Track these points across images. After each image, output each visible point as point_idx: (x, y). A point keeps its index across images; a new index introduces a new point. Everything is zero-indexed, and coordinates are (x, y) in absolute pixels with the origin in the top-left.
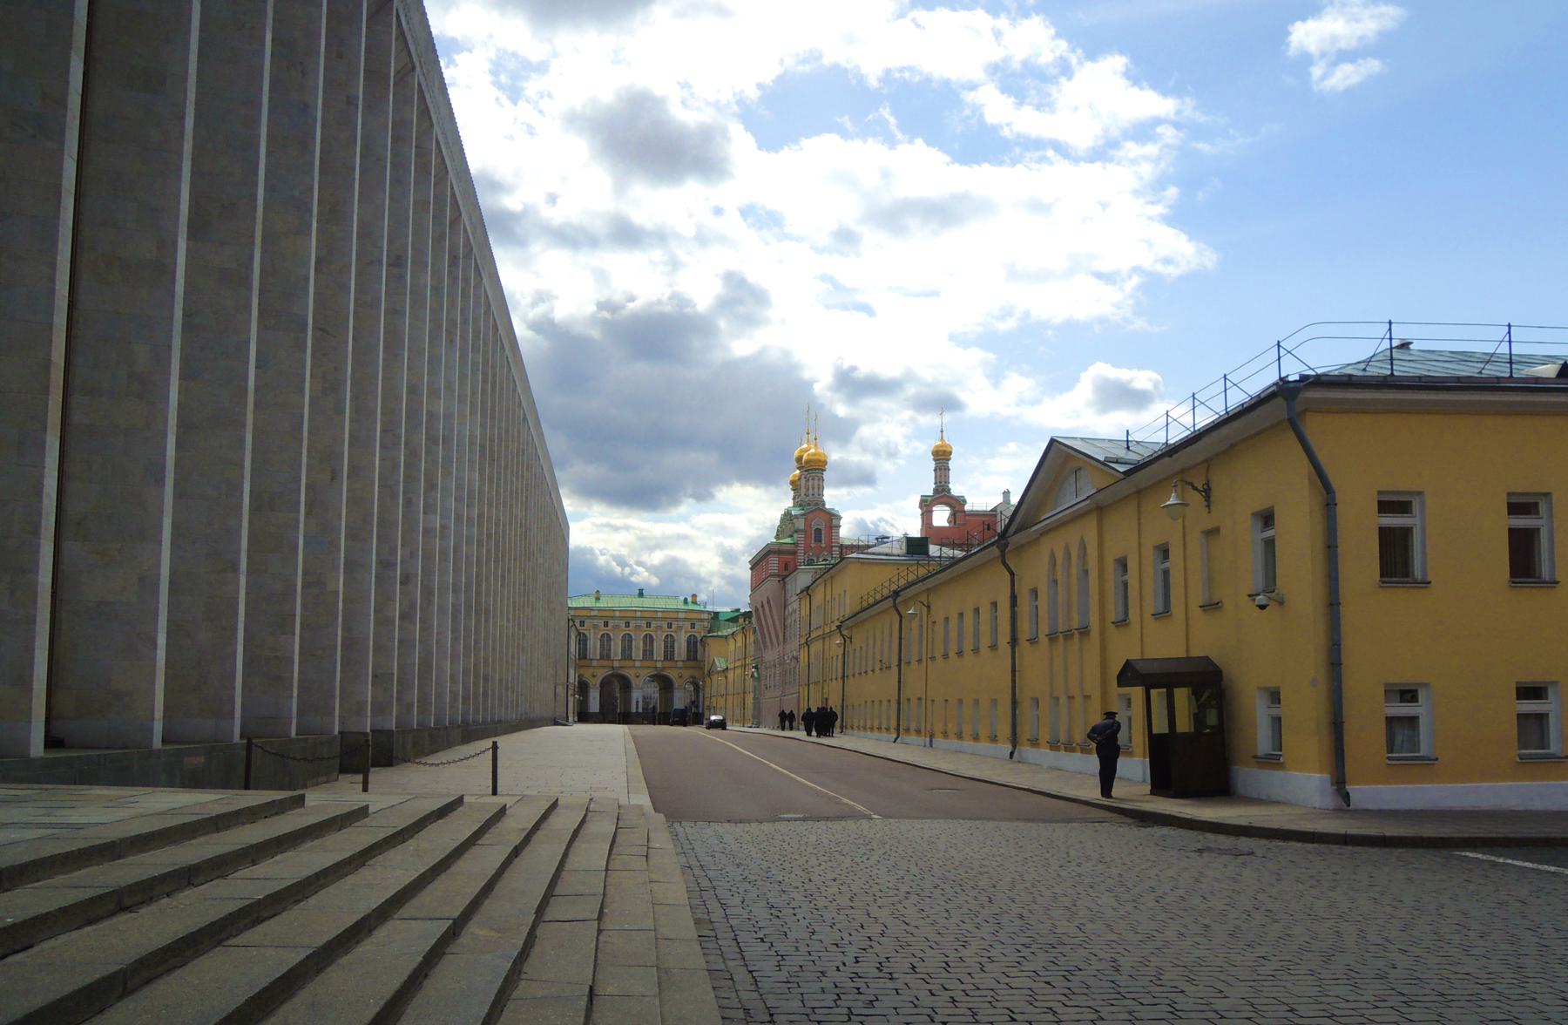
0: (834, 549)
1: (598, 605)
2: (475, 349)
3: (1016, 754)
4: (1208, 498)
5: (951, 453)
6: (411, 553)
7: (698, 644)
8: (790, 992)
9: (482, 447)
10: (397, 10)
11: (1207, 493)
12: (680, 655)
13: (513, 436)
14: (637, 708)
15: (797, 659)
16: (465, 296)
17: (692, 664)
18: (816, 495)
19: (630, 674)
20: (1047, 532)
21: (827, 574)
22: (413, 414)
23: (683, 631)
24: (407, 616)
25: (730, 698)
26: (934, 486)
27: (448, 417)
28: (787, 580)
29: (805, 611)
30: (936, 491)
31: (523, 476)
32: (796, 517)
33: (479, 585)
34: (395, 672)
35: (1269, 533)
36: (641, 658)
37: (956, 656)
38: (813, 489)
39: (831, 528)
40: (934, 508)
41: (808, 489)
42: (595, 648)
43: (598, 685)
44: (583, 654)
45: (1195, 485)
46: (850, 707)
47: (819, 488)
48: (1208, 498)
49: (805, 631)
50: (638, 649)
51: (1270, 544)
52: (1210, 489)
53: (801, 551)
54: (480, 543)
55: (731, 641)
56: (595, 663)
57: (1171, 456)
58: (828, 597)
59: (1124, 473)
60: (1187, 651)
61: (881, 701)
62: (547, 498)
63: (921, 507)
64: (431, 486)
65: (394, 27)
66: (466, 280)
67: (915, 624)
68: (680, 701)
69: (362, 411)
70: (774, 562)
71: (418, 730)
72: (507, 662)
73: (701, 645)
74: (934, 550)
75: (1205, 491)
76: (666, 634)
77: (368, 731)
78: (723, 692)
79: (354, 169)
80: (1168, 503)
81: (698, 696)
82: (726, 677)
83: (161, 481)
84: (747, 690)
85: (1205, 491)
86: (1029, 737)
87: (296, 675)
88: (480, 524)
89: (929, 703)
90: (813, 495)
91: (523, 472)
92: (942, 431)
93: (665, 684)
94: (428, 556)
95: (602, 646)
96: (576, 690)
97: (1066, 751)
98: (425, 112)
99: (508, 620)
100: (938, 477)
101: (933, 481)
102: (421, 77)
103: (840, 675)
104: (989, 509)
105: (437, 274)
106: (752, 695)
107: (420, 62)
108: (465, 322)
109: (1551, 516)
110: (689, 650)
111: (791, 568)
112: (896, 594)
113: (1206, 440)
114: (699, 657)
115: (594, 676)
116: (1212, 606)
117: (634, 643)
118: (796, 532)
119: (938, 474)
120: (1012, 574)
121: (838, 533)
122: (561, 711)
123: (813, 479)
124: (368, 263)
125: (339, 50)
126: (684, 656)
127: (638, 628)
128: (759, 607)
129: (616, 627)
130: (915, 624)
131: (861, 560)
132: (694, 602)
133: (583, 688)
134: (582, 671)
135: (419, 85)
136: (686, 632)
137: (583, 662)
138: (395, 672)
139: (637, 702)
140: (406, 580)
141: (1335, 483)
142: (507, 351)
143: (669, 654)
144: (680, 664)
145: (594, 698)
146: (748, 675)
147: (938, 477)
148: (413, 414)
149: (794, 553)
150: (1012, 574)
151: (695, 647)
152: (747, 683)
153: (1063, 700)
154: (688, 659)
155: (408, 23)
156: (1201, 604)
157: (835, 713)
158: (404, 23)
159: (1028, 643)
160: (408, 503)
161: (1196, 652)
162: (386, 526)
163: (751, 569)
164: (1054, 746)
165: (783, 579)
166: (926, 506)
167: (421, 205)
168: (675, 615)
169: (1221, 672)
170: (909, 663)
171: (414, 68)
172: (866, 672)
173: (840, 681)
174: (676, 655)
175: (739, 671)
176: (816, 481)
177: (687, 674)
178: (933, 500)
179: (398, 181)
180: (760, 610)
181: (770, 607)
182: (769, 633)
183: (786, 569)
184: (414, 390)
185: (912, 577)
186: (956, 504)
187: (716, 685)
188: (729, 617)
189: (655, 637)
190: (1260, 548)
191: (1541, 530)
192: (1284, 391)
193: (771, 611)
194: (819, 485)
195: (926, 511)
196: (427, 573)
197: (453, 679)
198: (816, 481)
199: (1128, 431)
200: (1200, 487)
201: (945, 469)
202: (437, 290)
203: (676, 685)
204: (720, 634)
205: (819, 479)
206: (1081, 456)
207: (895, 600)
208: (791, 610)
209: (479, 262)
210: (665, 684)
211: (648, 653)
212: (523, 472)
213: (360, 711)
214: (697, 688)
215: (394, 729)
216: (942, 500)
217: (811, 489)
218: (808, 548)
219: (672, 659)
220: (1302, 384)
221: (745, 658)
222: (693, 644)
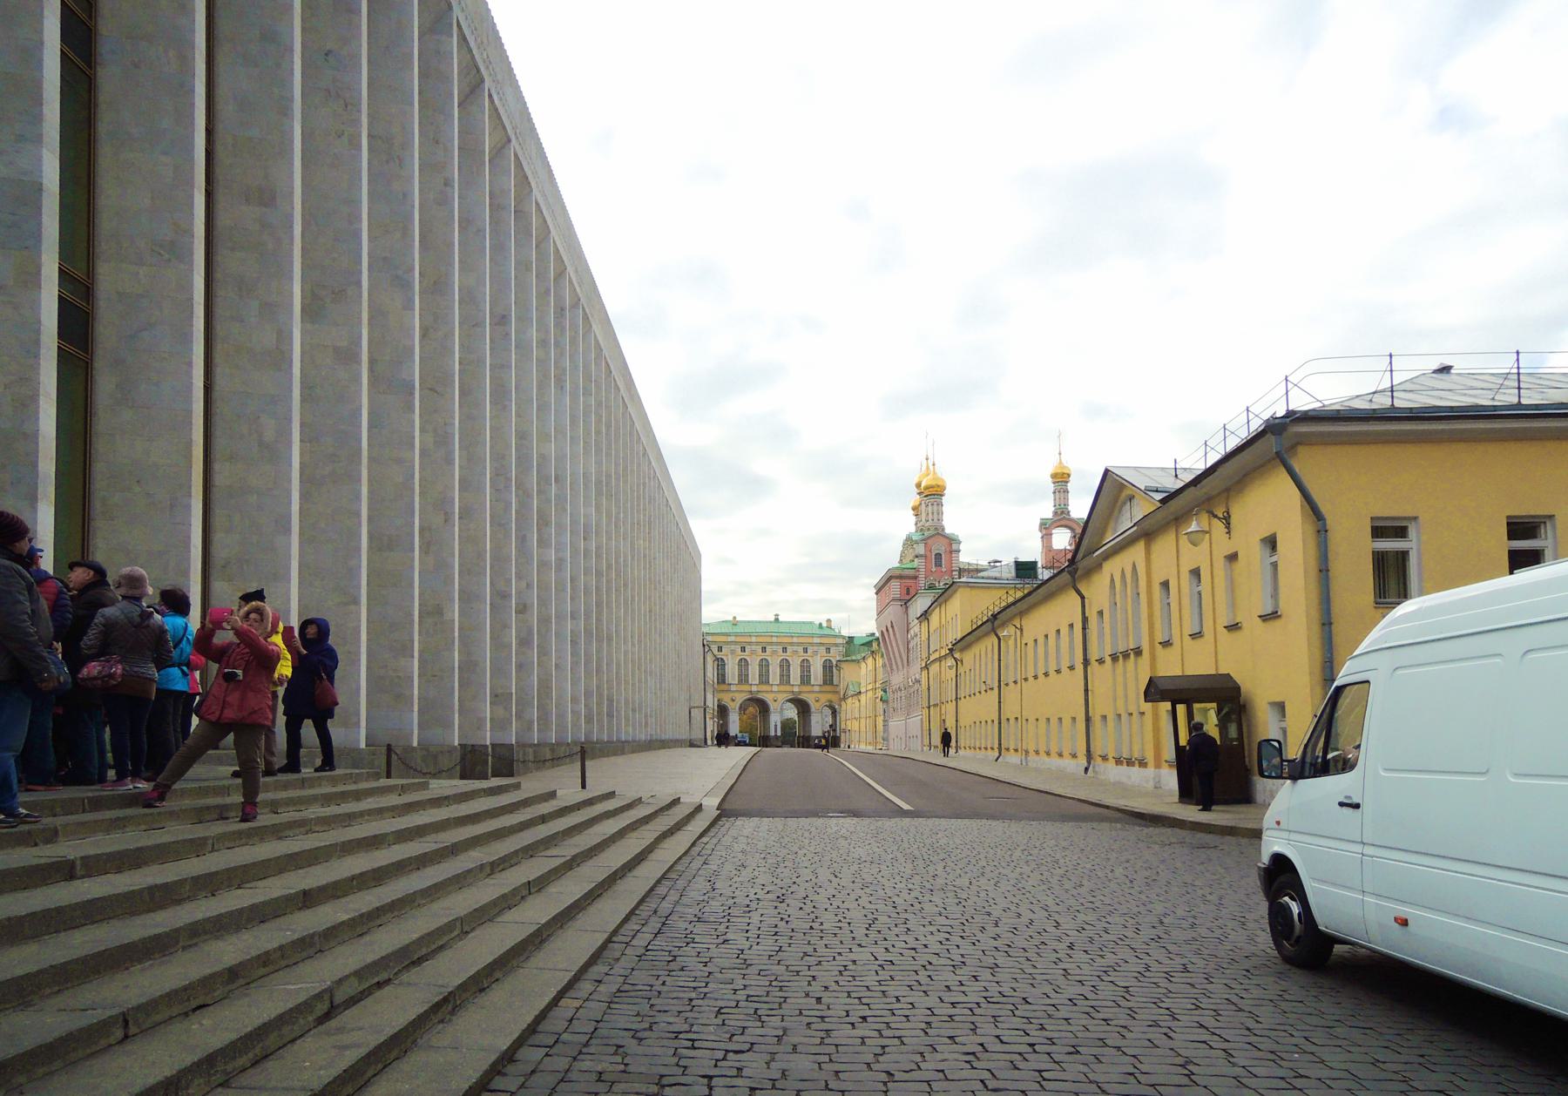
0: (954, 573)
1: (735, 631)
2: (587, 393)
3: (1091, 769)
4: (1228, 525)
5: (1069, 475)
6: (527, 584)
8: (1035, 1051)
9: (598, 482)
10: (489, 90)
11: (1227, 520)
12: (816, 679)
13: (632, 471)
14: (776, 731)
15: (918, 681)
16: (573, 341)
17: (828, 688)
19: (768, 698)
20: (1107, 556)
21: (944, 595)
22: (523, 460)
24: (524, 642)
25: (863, 721)
26: (1053, 509)
27: (560, 458)
29: (924, 636)
31: (645, 510)
32: (917, 542)
33: (599, 613)
34: (514, 691)
35: (1274, 559)
36: (778, 683)
37: (1033, 679)
38: (933, 513)
39: (951, 552)
43: (737, 708)
44: (722, 679)
45: (1216, 513)
46: (963, 727)
47: (938, 514)
48: (1228, 525)
49: (925, 655)
50: (775, 673)
51: (1275, 565)
52: (1230, 516)
53: (922, 576)
54: (599, 574)
55: (863, 665)
56: (733, 688)
57: (1195, 486)
58: (943, 620)
59: (1161, 501)
60: (1217, 670)
61: (986, 722)
62: (674, 528)
64: (544, 521)
65: (487, 105)
66: (574, 327)
67: (1011, 642)
68: (818, 725)
69: (472, 459)
70: (895, 588)
71: (539, 745)
72: (633, 685)
75: (1225, 518)
77: (488, 743)
78: (857, 716)
79: (189, 424)
80: (1189, 530)
81: (836, 721)
82: (859, 701)
83: (288, 531)
84: (878, 714)
85: (1225, 518)
86: (1100, 753)
87: (416, 692)
88: (598, 556)
89: (1024, 721)
91: (644, 504)
92: (1060, 454)
93: (803, 707)
94: (544, 587)
95: (740, 670)
96: (716, 713)
97: (1128, 765)
98: (523, 181)
99: (633, 645)
101: (1053, 504)
102: (517, 147)
103: (954, 698)
105: (543, 327)
106: (882, 717)
107: (516, 134)
108: (575, 368)
109: (1555, 537)
111: (912, 592)
112: (995, 616)
113: (1220, 470)
114: (835, 683)
115: (733, 700)
116: (1234, 627)
117: (770, 667)
118: (917, 557)
119: (1057, 497)
120: (1083, 598)
122: (697, 735)
123: (932, 505)
124: (471, 324)
125: (434, 138)
127: (774, 652)
129: (753, 652)
130: (1011, 642)
131: (970, 585)
132: (829, 627)
133: (723, 711)
134: (721, 696)
135: (516, 155)
137: (723, 687)
138: (514, 691)
139: (776, 726)
140: (523, 609)
141: (1324, 508)
142: (622, 391)
143: (805, 679)
144: (817, 689)
145: (734, 722)
146: (877, 698)
148: (523, 460)
149: (916, 578)
150: (1083, 598)
152: (878, 707)
153: (1124, 717)
154: (825, 683)
155: (501, 99)
156: (1226, 625)
157: (949, 734)
158: (497, 102)
159: (1097, 663)
160: (522, 539)
162: (500, 560)
163: (877, 593)
164: (1118, 761)
165: (905, 604)
167: (523, 266)
169: (1239, 688)
170: (1007, 685)
171: (509, 141)
172: (974, 694)
173: (954, 702)
174: (791, 679)
175: (870, 694)
176: (935, 507)
177: (824, 698)
178: (1052, 524)
179: (499, 248)
180: (890, 630)
181: (894, 631)
182: (895, 657)
183: (908, 594)
184: (522, 436)
185: (1011, 600)
187: (849, 708)
188: (864, 642)
189: (791, 663)
190: (1269, 569)
191: (1410, 553)
192: (1273, 428)
193: (895, 635)
195: (1045, 535)
196: (543, 603)
197: (575, 700)
198: (935, 507)
202: (543, 343)
203: (813, 710)
204: (854, 658)
205: (938, 505)
207: (993, 623)
209: (587, 310)
210: (803, 707)
211: (785, 678)
212: (644, 504)
213: (480, 724)
214: (834, 713)
215: (514, 742)
216: (1063, 523)
217: (930, 515)
218: (928, 573)
219: (788, 682)
220: (1288, 420)
221: (875, 682)
222: (828, 668)
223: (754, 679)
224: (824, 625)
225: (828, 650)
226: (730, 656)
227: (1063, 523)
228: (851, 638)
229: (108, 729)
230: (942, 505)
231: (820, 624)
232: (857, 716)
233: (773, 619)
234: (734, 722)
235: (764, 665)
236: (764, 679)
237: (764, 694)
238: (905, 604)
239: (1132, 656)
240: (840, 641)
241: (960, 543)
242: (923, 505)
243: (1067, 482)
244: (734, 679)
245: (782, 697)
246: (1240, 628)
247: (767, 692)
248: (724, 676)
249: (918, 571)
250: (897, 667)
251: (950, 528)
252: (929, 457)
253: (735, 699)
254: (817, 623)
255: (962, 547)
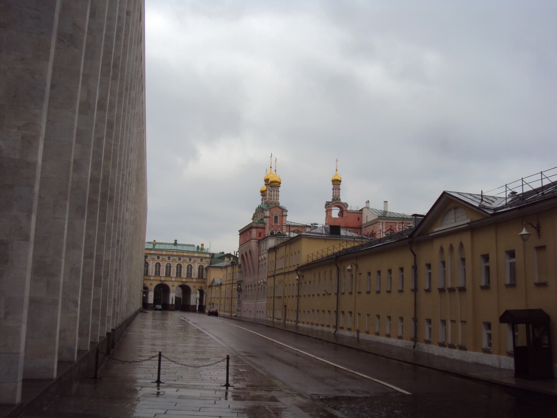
0: (284, 227)
7: (204, 270)
12: (195, 275)
14: (172, 302)
18: (275, 199)
23: (197, 263)
25: (223, 301)
26: (332, 197)
28: (260, 242)
30: (333, 200)
36: (186, 277)
38: (274, 196)
39: (282, 216)
40: (333, 208)
41: (271, 196)
42: (152, 270)
44: (146, 273)
47: (277, 196)
52: (540, 227)
63: (326, 207)
73: (205, 270)
74: (343, 232)
76: (156, 262)
82: (221, 288)
90: (274, 199)
93: (186, 290)
100: (335, 193)
101: (332, 195)
104: (359, 210)
110: (199, 274)
114: (204, 277)
119: (335, 192)
121: (286, 219)
123: (274, 191)
126: (196, 276)
128: (244, 255)
131: (308, 236)
134: (146, 282)
136: (198, 263)
137: (146, 277)
139: (172, 299)
143: (189, 275)
147: (335, 193)
149: (264, 228)
150: (415, 255)
151: (202, 271)
161: (533, 307)
163: (240, 234)
166: (328, 206)
168: (182, 254)
176: (275, 193)
177: (198, 286)
180: (248, 255)
186: (342, 207)
189: (193, 266)
194: (277, 194)
198: (275, 193)
199: (482, 191)
200: (535, 226)
201: (338, 189)
203: (192, 291)
206: (462, 202)
208: (263, 257)
211: (179, 274)
219: (191, 277)
222: (201, 268)
223: (163, 274)
224: (200, 247)
225: (202, 260)
226: (151, 261)
227: (337, 204)
228: (213, 254)
229: (547, 346)
230: (279, 192)
231: (198, 246)
232: (276, 300)
233: (173, 242)
234: (151, 296)
235: (169, 267)
236: (168, 274)
237: (189, 283)
238: (259, 241)
239: (264, 260)
240: (208, 256)
241: (287, 211)
242: (268, 190)
243: (340, 184)
244: (152, 273)
245: (177, 284)
246: (547, 285)
247: (169, 281)
248: (159, 272)
249: (266, 225)
250: (250, 271)
251: (282, 203)
252: (272, 166)
253: (152, 286)
254: (196, 245)
255: (288, 213)
